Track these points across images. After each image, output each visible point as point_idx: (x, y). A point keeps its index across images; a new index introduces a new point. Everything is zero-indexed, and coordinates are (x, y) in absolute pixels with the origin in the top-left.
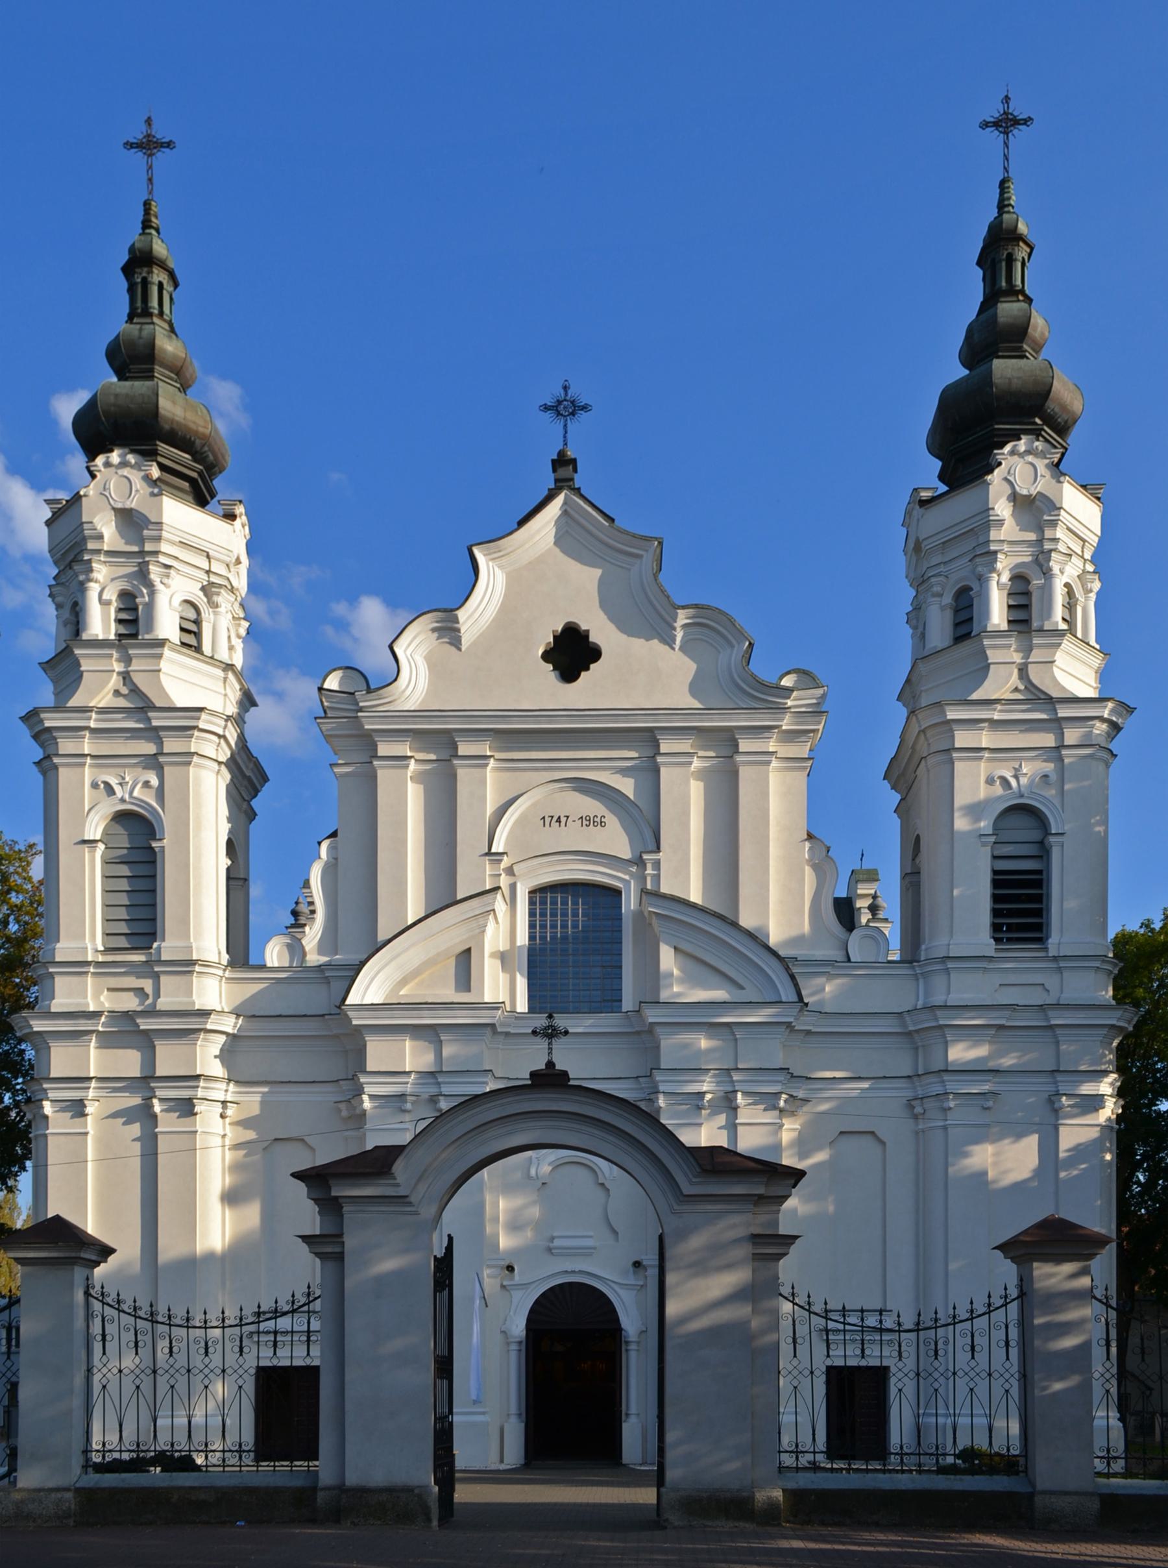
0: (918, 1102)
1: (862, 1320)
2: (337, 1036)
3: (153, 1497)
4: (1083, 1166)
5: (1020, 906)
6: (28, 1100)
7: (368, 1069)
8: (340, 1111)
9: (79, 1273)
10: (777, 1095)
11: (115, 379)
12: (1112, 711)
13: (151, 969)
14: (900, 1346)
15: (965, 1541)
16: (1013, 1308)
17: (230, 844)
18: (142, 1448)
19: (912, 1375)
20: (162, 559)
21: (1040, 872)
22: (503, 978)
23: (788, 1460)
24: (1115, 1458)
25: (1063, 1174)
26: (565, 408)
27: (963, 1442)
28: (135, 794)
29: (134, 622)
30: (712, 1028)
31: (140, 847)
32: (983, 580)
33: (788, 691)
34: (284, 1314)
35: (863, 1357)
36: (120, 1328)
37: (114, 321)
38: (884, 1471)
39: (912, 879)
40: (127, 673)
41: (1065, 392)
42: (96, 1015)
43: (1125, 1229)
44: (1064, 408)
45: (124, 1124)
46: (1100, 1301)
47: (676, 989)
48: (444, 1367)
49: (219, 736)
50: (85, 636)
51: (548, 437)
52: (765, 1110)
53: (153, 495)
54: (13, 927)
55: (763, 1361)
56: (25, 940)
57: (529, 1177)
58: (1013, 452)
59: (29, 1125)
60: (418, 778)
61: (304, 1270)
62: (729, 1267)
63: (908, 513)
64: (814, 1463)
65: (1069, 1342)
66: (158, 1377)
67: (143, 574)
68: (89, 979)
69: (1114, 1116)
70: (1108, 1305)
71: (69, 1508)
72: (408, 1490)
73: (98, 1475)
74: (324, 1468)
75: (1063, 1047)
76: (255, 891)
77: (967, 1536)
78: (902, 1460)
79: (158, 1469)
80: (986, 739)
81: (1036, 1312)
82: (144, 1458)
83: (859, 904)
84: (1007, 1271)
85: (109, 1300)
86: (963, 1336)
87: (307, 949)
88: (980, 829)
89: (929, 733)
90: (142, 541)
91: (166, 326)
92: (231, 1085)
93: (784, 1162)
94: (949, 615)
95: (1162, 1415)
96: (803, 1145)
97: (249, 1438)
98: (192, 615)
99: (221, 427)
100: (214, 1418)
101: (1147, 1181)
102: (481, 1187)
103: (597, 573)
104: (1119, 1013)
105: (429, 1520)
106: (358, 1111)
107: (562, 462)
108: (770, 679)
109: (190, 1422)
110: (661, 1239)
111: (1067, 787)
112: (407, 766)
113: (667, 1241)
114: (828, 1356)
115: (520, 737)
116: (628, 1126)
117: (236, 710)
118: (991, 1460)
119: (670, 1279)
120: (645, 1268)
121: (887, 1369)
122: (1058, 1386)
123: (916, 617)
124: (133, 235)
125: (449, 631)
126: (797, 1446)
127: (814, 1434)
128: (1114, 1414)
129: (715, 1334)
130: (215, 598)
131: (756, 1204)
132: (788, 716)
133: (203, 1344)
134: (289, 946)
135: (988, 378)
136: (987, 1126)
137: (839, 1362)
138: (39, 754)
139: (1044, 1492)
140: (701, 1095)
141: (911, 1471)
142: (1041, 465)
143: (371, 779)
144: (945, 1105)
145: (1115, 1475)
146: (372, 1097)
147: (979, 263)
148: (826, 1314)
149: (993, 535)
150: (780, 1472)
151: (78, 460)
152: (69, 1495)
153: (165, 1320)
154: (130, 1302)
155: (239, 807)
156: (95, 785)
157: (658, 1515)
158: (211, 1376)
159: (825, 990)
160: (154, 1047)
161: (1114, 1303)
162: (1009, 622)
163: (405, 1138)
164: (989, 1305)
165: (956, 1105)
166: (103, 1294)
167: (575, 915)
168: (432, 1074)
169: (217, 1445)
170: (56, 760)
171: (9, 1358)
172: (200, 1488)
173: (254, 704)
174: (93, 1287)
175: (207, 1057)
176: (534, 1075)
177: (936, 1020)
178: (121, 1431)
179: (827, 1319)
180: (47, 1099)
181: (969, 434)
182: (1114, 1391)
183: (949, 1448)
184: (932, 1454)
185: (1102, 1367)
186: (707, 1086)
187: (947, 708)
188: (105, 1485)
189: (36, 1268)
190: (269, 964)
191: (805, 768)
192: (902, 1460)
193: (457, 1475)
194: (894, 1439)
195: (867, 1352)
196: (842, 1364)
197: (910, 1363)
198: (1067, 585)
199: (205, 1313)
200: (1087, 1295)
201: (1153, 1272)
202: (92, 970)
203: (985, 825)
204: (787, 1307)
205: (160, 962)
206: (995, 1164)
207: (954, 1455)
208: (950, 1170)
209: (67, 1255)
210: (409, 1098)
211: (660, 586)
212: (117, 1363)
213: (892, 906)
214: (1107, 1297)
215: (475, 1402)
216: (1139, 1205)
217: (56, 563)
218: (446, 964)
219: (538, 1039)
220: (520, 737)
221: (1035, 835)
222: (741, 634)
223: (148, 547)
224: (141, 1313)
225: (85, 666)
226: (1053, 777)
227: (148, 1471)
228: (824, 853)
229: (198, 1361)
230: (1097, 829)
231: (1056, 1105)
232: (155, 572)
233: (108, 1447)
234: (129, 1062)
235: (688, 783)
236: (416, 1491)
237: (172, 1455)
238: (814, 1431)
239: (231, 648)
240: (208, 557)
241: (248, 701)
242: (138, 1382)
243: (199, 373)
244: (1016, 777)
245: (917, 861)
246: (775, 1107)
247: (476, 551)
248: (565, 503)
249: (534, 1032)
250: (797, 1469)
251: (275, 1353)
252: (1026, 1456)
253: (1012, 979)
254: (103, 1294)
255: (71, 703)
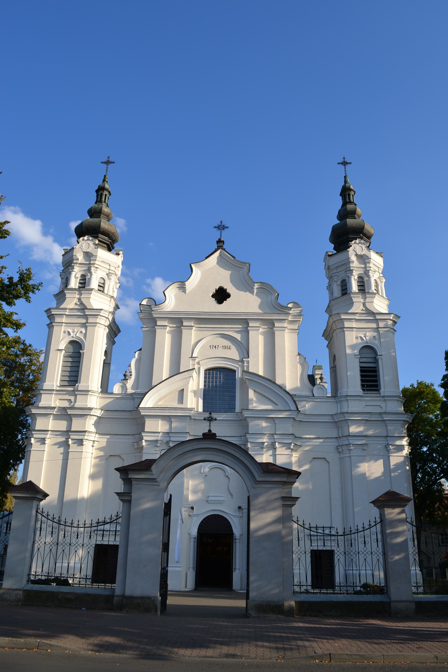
0: (340, 447)
1: (324, 531)
2: (135, 418)
3: (52, 595)
4: (399, 471)
5: (370, 378)
6: (27, 438)
7: (145, 431)
8: (134, 445)
9: (35, 503)
10: (290, 444)
11: (89, 218)
12: (393, 317)
13: (74, 393)
14: (338, 542)
15: (365, 623)
16: (379, 526)
17: (106, 352)
18: (50, 575)
19: (343, 553)
20: (95, 266)
21: (375, 367)
22: (194, 399)
23: (297, 589)
24: (420, 586)
25: (392, 474)
26: (221, 227)
27: (363, 581)
28: (77, 335)
29: (84, 283)
30: (267, 419)
31: (76, 352)
32: (349, 278)
33: (290, 308)
34: (108, 523)
35: (324, 546)
36: (47, 526)
37: (91, 202)
38: (333, 593)
39: (334, 369)
40: (80, 298)
41: (368, 227)
42: (54, 408)
43: (416, 495)
44: (368, 232)
45: (58, 448)
46: (409, 523)
47: (254, 405)
48: (166, 547)
49: (106, 318)
50: (69, 287)
51: (216, 235)
52: (286, 449)
53: (95, 248)
54: (31, 377)
55: (286, 548)
56: (34, 382)
57: (201, 473)
58: (355, 243)
59: (25, 447)
60: (169, 332)
61: (116, 506)
62: (274, 509)
63: (325, 259)
64: (307, 590)
65: (399, 540)
66: (59, 546)
67: (89, 270)
68: (53, 396)
69: (408, 453)
70: (413, 525)
71: (20, 598)
72: (149, 598)
73: (32, 585)
74: (117, 587)
75: (389, 428)
76: (112, 367)
77: (366, 620)
78: (340, 589)
79: (55, 584)
80: (354, 325)
81: (387, 528)
82: (50, 579)
83: (317, 377)
84: (375, 511)
85: (44, 514)
86: (361, 537)
87: (128, 388)
88: (355, 353)
89: (336, 322)
90: (90, 260)
91: (106, 205)
92: (97, 435)
93: (293, 469)
94: (340, 288)
95: (435, 568)
96: (300, 462)
97: (90, 573)
98: (103, 282)
99: (118, 230)
100: (77, 564)
101: (422, 477)
102: (183, 476)
103: (230, 272)
104: (406, 416)
105: (157, 611)
106: (140, 446)
107: (220, 242)
108: (284, 304)
109: (68, 565)
110: (249, 497)
111: (381, 340)
112: (166, 329)
113: (251, 499)
114: (311, 546)
115: (204, 320)
116: (236, 454)
117: (113, 310)
118: (374, 588)
119: (252, 514)
120: (243, 509)
121: (333, 551)
122: (397, 557)
123: (330, 287)
124: (100, 183)
125: (182, 288)
126: (300, 583)
127: (306, 578)
128: (418, 568)
129: (269, 536)
130: (110, 277)
131: (283, 485)
132: (290, 316)
133: (76, 534)
134: (122, 386)
135: (346, 223)
136: (365, 456)
137: (315, 548)
138: (48, 322)
139: (394, 601)
140: (263, 443)
141: (344, 593)
142: (364, 247)
143: (154, 332)
144: (350, 448)
145: (420, 593)
146: (146, 441)
147: (340, 195)
148: (310, 529)
149: (351, 265)
150: (294, 594)
151: (75, 238)
152: (21, 592)
153: (64, 523)
154: (52, 516)
155: (110, 340)
156: (65, 332)
157: (246, 612)
158: (78, 547)
159: (306, 406)
160: (72, 420)
161: (414, 524)
162: (359, 290)
163: (156, 457)
164: (370, 525)
165: (353, 448)
166: (42, 512)
167: (220, 378)
168: (168, 433)
169: (78, 576)
170: (53, 324)
171: (6, 535)
172: (70, 593)
173: (119, 308)
174: (39, 509)
175: (90, 424)
176: (204, 434)
177: (345, 417)
178: (43, 568)
179: (310, 531)
180: (33, 437)
181: (344, 235)
182: (417, 559)
183: (358, 584)
184: (351, 586)
185: (412, 549)
186: (265, 440)
187: (341, 315)
188: (34, 589)
189: (20, 500)
190: (114, 393)
191: (296, 332)
192: (340, 589)
193: (168, 592)
194: (337, 580)
195: (326, 544)
196: (317, 549)
197: (342, 548)
198: (375, 280)
199: (78, 521)
200: (404, 521)
201: (427, 511)
202: (55, 392)
203: (356, 352)
204: (295, 526)
205: (78, 391)
206: (368, 470)
207: (360, 586)
208: (353, 473)
209: (32, 496)
210: (159, 442)
211: (249, 277)
212: (45, 540)
213: (327, 377)
214: (412, 522)
215: (177, 562)
216: (420, 486)
217: (63, 266)
218: (175, 395)
219: (206, 421)
220: (204, 320)
221: (373, 356)
222: (275, 291)
223: (92, 262)
224: (55, 520)
225: (67, 296)
226: (377, 337)
227: (51, 585)
228: (304, 359)
229: (74, 540)
230: (393, 354)
231: (388, 449)
232: (93, 269)
233: (37, 574)
234: (62, 425)
235: (258, 336)
236: (152, 599)
237: (61, 579)
238: (306, 577)
239: (113, 291)
240: (110, 265)
241: (117, 307)
242: (51, 548)
243: (113, 217)
244: (365, 337)
245: (335, 363)
246: (289, 448)
247: (192, 265)
248: (220, 253)
249: (204, 419)
250: (300, 593)
251: (103, 539)
252: (387, 586)
253: (369, 403)
254: (42, 512)
255: (61, 307)
